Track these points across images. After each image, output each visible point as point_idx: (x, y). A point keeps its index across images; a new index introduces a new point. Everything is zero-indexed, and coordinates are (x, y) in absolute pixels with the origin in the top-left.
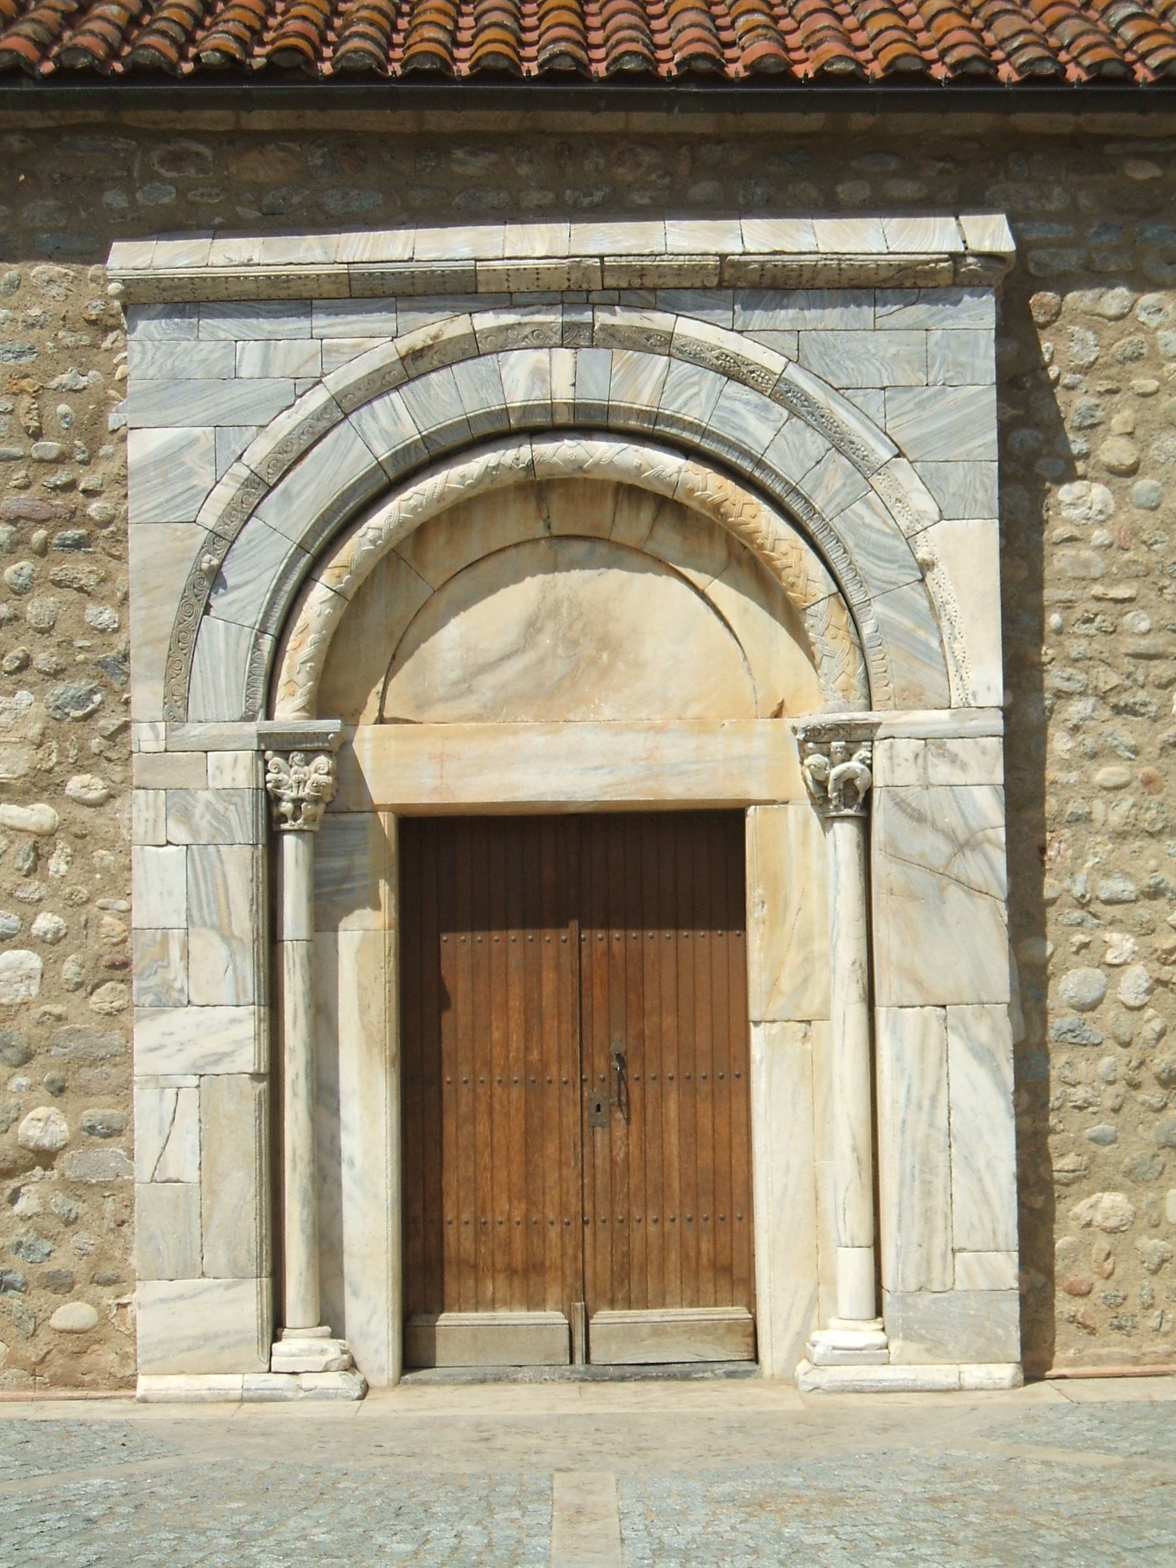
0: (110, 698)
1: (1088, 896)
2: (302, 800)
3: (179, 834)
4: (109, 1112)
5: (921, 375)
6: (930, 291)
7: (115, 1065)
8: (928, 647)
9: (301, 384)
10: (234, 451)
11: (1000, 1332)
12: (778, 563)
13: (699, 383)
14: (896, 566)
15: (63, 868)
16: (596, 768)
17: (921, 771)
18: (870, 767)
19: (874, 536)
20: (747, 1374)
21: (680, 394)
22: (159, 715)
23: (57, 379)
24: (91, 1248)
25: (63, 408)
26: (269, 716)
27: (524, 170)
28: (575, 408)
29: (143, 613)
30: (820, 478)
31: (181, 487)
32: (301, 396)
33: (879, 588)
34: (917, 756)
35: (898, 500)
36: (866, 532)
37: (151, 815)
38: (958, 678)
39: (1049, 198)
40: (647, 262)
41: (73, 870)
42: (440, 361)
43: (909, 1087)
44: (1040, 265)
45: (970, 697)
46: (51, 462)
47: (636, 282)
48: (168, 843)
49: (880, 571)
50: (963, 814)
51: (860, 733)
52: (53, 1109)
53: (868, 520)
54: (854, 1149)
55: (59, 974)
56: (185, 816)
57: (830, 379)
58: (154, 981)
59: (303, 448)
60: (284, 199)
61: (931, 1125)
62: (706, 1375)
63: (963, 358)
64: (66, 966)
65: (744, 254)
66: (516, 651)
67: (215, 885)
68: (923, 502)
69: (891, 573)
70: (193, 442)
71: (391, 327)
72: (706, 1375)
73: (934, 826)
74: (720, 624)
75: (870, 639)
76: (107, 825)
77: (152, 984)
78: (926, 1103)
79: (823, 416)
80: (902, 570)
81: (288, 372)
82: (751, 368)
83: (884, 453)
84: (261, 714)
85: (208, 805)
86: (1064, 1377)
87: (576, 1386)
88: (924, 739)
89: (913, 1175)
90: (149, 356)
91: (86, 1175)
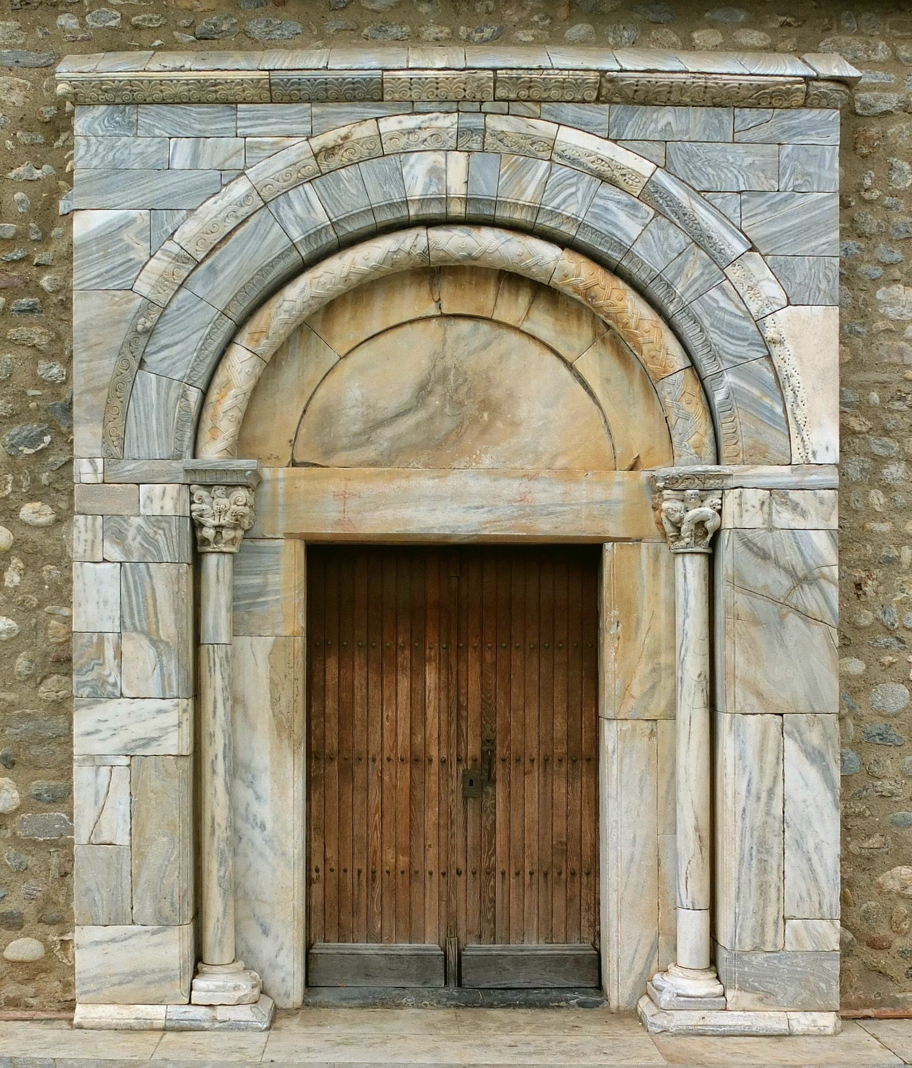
0: (59, 439)
1: (896, 625)
2: (222, 527)
3: (114, 552)
4: (53, 783)
5: (773, 182)
6: (784, 111)
7: (60, 744)
8: (773, 413)
9: (225, 175)
10: (166, 231)
11: (823, 985)
12: (641, 340)
13: (576, 184)
14: (746, 344)
15: (17, 579)
16: (477, 508)
17: (766, 516)
18: (720, 512)
19: (727, 318)
20: (597, 1004)
21: (559, 193)
22: (98, 452)
23: (14, 171)
24: (39, 894)
25: (19, 196)
26: (194, 456)
29: (84, 365)
30: (680, 270)
31: (119, 260)
32: (225, 185)
33: (731, 362)
34: (763, 504)
35: (751, 288)
36: (721, 314)
37: (89, 536)
38: (799, 439)
40: (535, 75)
41: (25, 581)
42: (350, 160)
43: (749, 781)
44: (865, 106)
45: (810, 456)
46: (8, 240)
48: (105, 560)
49: (732, 348)
50: (802, 554)
51: (711, 483)
52: (7, 779)
53: (722, 304)
54: (697, 829)
55: (12, 667)
56: (119, 537)
57: (693, 183)
58: (90, 676)
59: (228, 230)
60: (215, 25)
61: (768, 814)
62: (561, 1004)
63: (811, 170)
64: (19, 660)
65: (621, 71)
66: (410, 410)
67: (145, 597)
68: (772, 289)
69: (742, 349)
70: (131, 222)
71: (307, 128)
72: (561, 1004)
73: (777, 563)
74: (584, 393)
75: (722, 404)
76: (54, 545)
77: (89, 678)
78: (764, 796)
79: (685, 214)
80: (751, 347)
81: (215, 165)
82: (623, 172)
83: (739, 247)
84: (188, 454)
87: (452, 1010)
88: (770, 490)
89: (751, 855)
90: (93, 149)
91: (33, 835)
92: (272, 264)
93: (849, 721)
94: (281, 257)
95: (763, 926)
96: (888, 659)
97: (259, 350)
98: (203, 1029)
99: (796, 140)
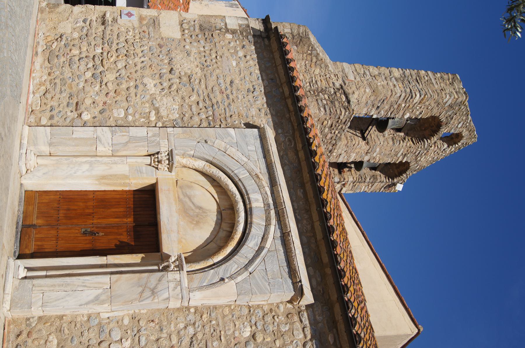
8: (204, 282)
11: (19, 305)
27: (301, 203)
28: (251, 208)
30: (242, 257)
39: (319, 316)
40: (286, 216)
47: (281, 216)
61: (78, 286)
63: (276, 286)
73: (158, 284)
78: (84, 284)
85: (156, 140)
86: (4, 329)
92: (227, 167)
93: (108, 321)
94: (230, 169)
95: (41, 286)
96: (129, 332)
97: (205, 167)
98: (20, 150)
99: (284, 282)
